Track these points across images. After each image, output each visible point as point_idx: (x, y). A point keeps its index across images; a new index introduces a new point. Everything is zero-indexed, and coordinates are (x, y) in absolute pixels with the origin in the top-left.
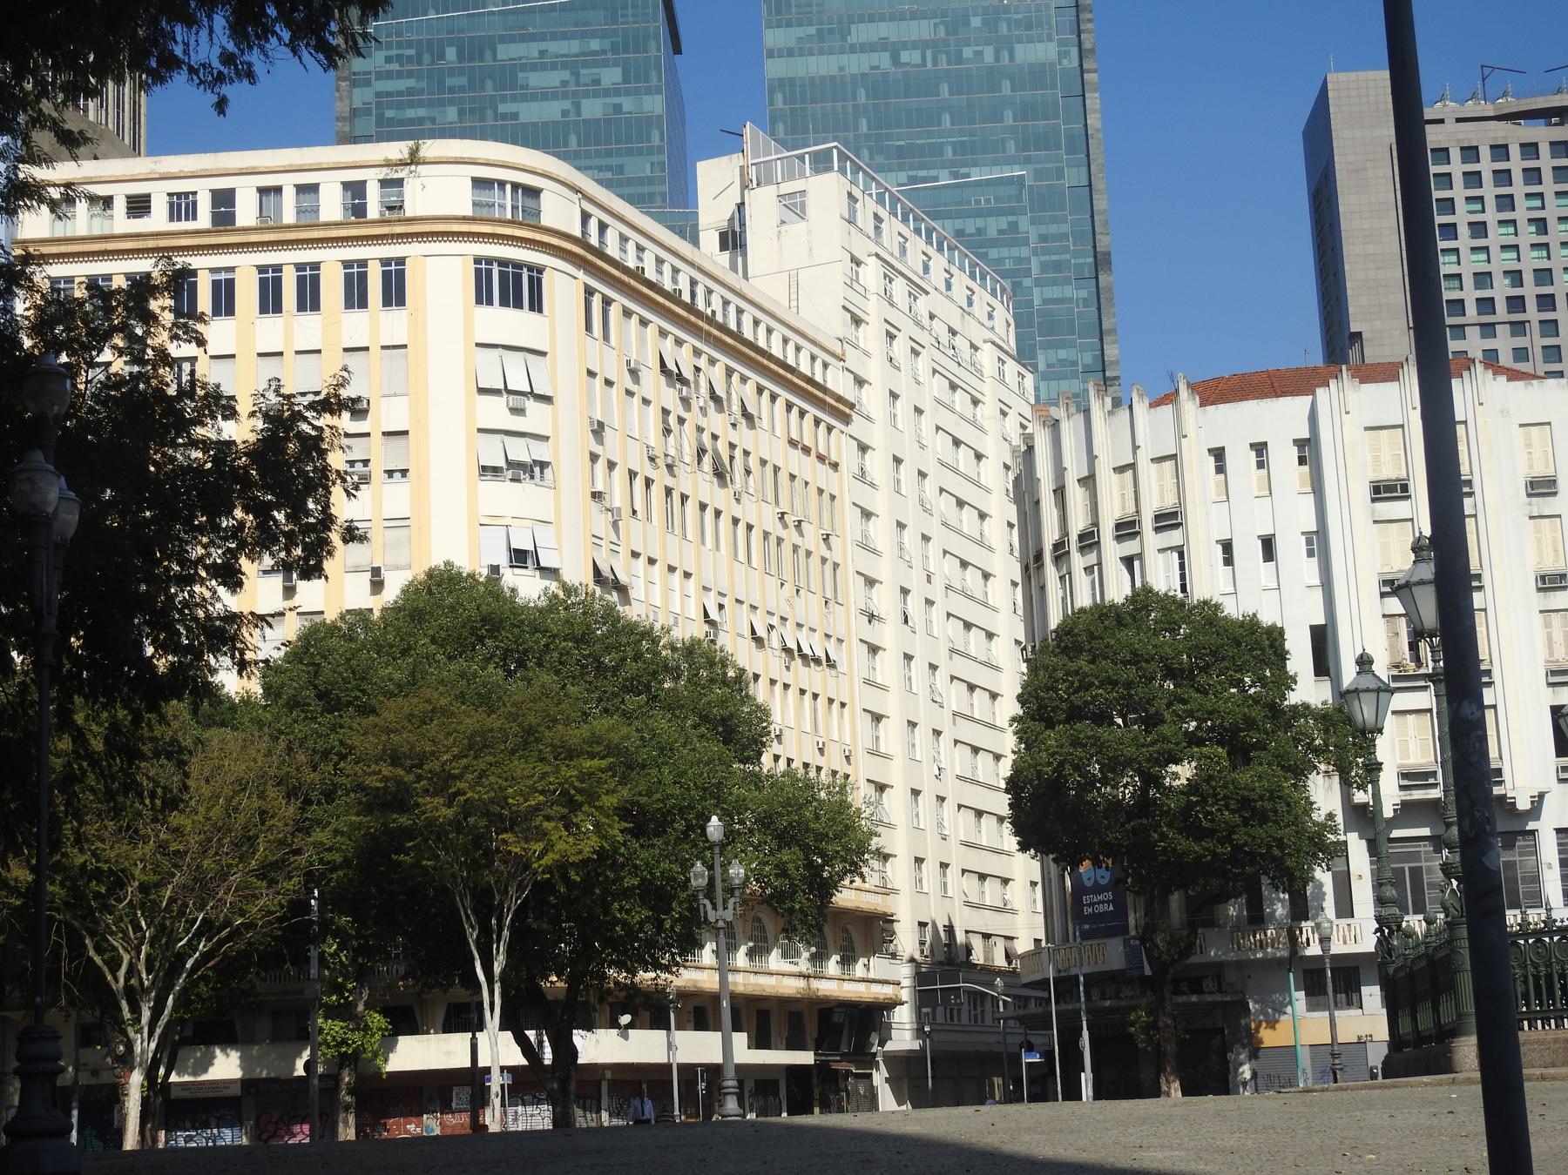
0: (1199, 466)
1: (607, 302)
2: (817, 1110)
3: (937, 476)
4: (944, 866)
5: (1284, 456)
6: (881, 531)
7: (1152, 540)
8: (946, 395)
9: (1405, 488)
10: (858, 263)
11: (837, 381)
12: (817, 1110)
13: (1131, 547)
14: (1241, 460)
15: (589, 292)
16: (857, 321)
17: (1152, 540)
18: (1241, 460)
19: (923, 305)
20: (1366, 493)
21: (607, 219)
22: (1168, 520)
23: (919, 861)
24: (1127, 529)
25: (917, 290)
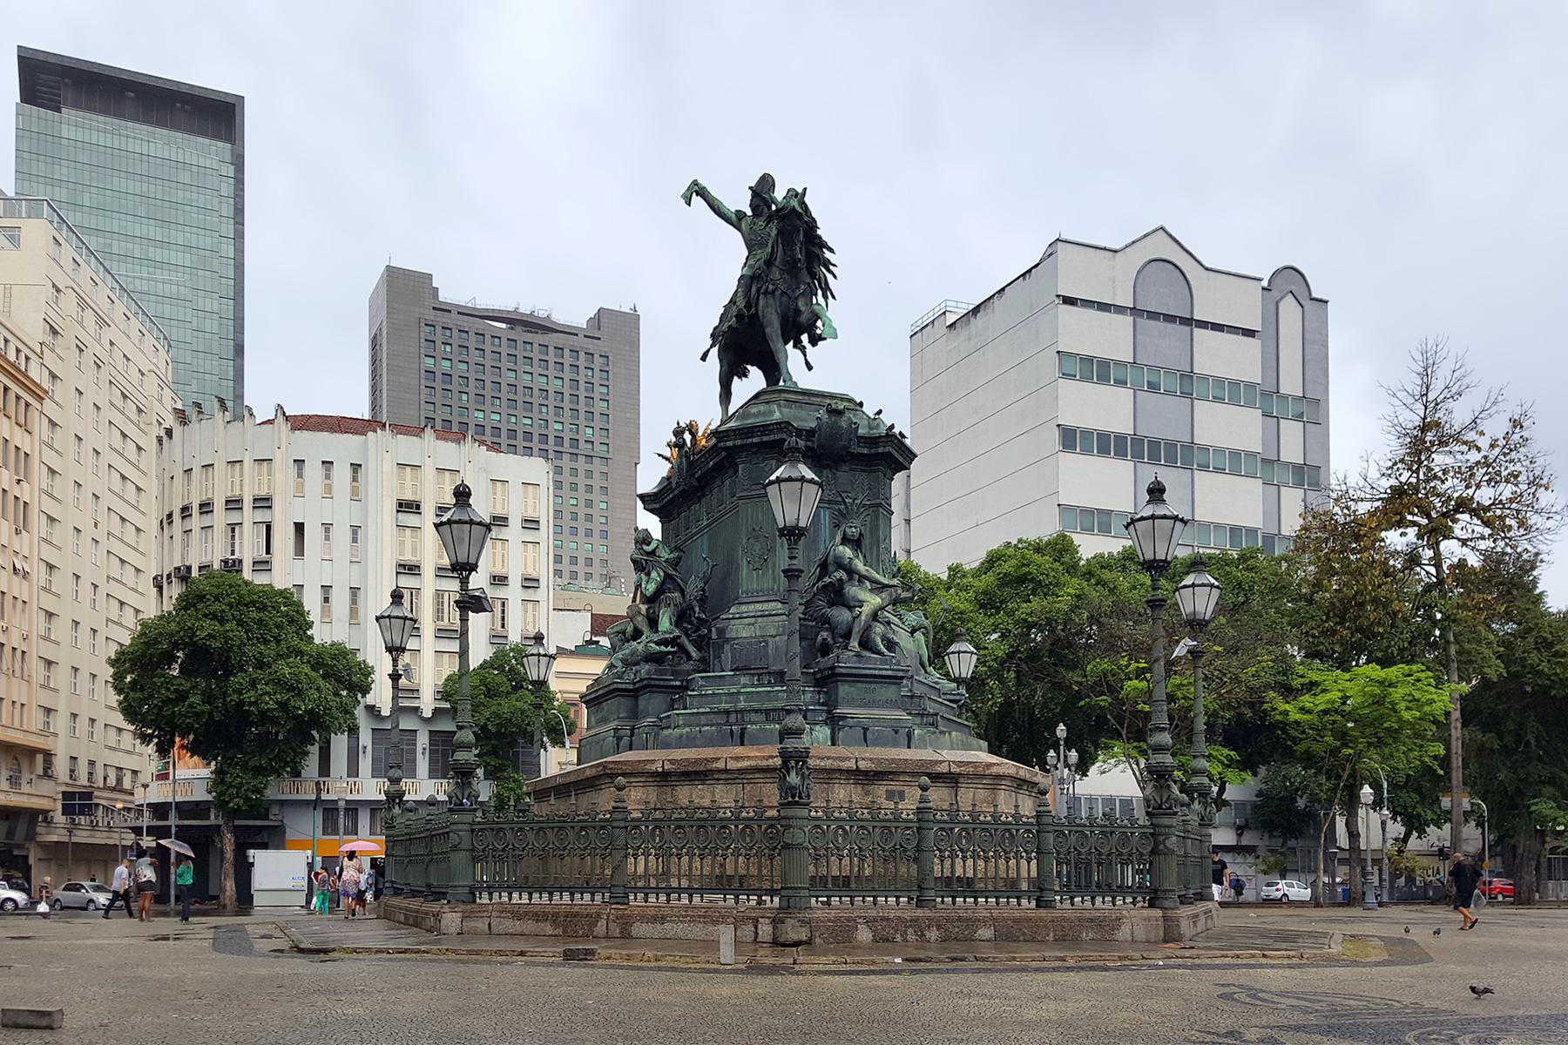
0: (283, 472)
1: (27, 405)
2: (342, 804)
3: (108, 457)
4: (93, 721)
5: (342, 473)
6: (62, 487)
7: (248, 515)
8: (119, 402)
9: (418, 507)
10: (58, 290)
11: (35, 372)
12: (342, 804)
13: (234, 517)
14: (313, 471)
15: (6, 389)
16: (54, 332)
17: (248, 515)
18: (313, 471)
19: (108, 334)
20: (391, 506)
21: (21, 347)
22: (263, 502)
23: (75, 716)
24: (233, 504)
25: (102, 322)
